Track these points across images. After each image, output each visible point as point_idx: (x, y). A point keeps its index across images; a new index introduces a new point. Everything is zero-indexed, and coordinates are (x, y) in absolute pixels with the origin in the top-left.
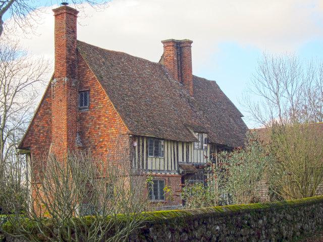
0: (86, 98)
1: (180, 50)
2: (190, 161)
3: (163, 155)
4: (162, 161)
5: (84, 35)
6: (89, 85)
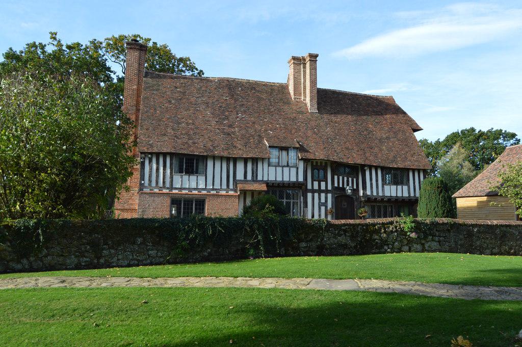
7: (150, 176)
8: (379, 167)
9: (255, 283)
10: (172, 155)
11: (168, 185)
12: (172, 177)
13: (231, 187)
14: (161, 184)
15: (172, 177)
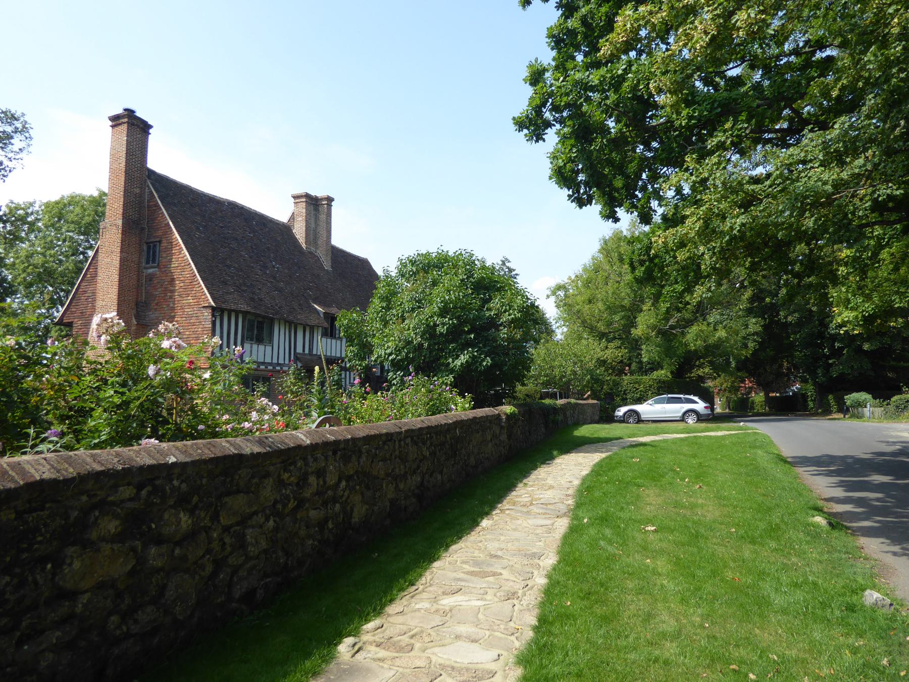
0: (154, 252)
1: (317, 207)
2: (315, 352)
3: (271, 341)
4: (269, 349)
5: (159, 160)
6: (160, 233)
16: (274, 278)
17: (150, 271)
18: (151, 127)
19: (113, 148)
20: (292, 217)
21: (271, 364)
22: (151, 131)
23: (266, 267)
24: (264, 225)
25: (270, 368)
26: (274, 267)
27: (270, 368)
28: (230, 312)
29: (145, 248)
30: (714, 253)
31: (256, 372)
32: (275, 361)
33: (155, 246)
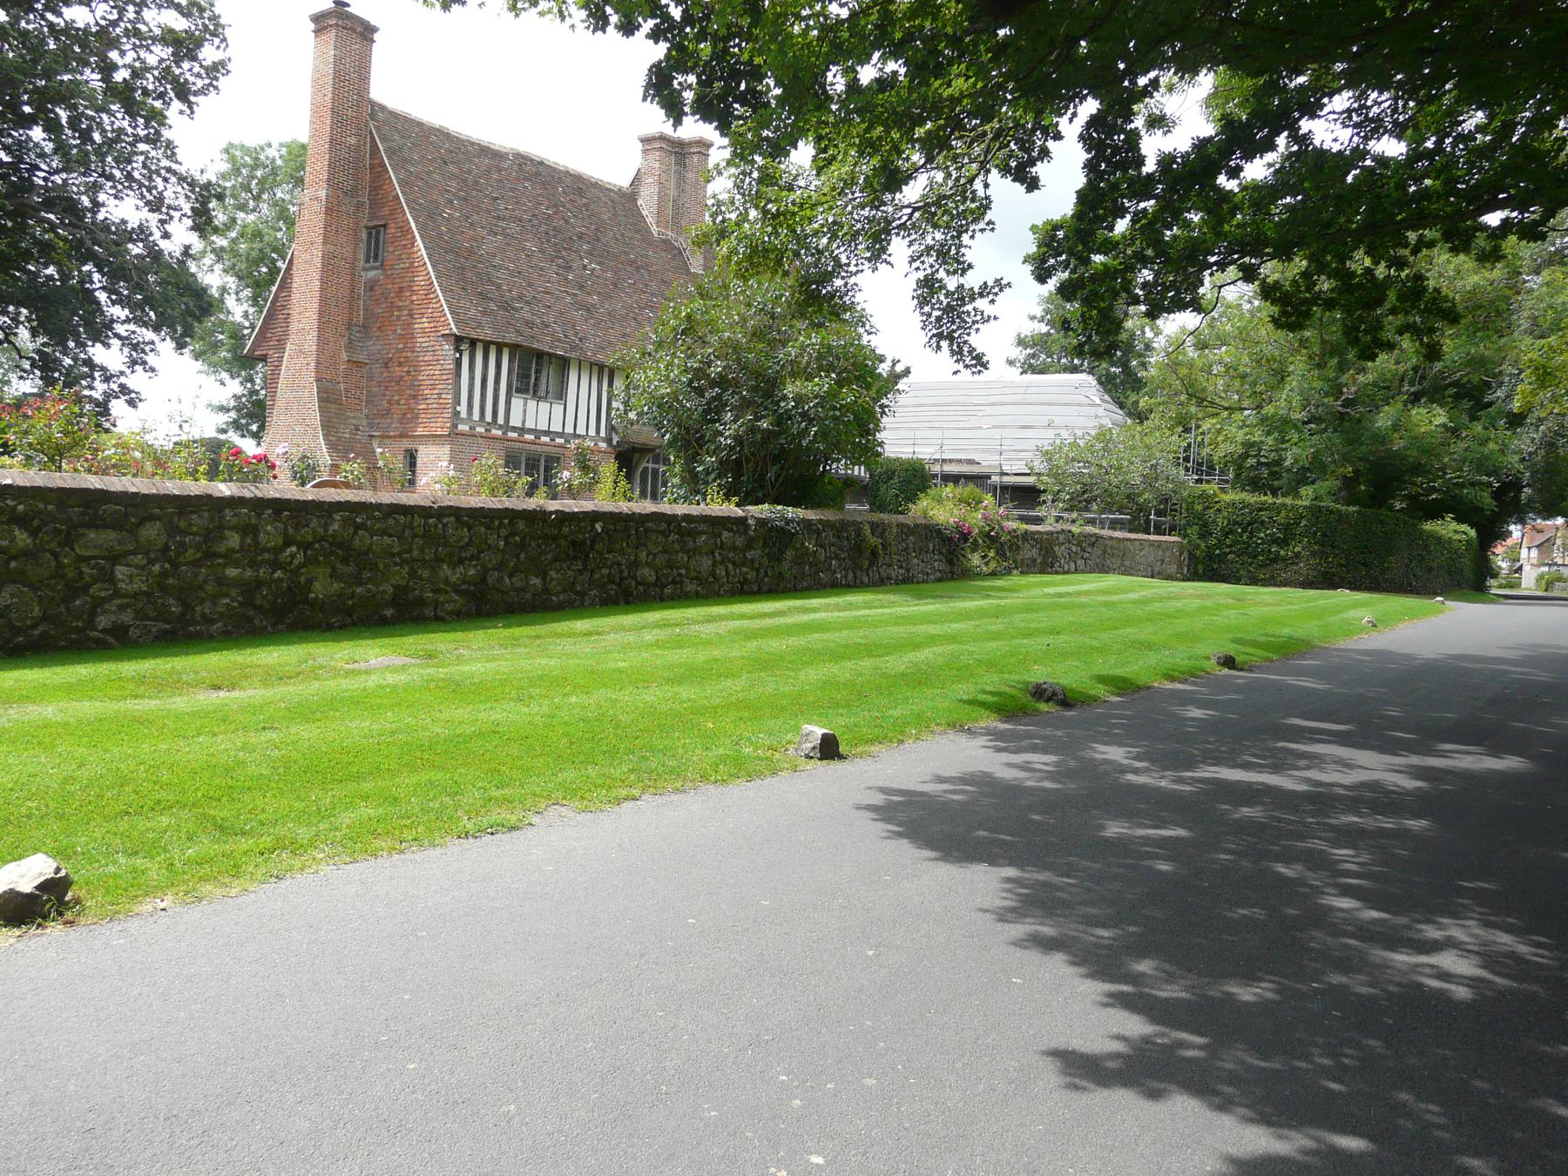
3: (561, 395)
5: (394, 85)
7: (470, 397)
8: (506, 345)
9: (1291, 680)
10: (514, 348)
11: (501, 421)
12: (508, 403)
13: (603, 434)
14: (489, 418)
15: (508, 403)
16: (582, 287)
17: (372, 274)
18: (374, 30)
19: (316, 70)
20: (637, 180)
21: (561, 435)
22: (376, 37)
23: (568, 268)
24: (580, 192)
25: (560, 441)
26: (585, 267)
27: (560, 441)
28: (487, 345)
29: (364, 236)
30: (141, 46)
31: (533, 447)
32: (569, 430)
33: (378, 233)
